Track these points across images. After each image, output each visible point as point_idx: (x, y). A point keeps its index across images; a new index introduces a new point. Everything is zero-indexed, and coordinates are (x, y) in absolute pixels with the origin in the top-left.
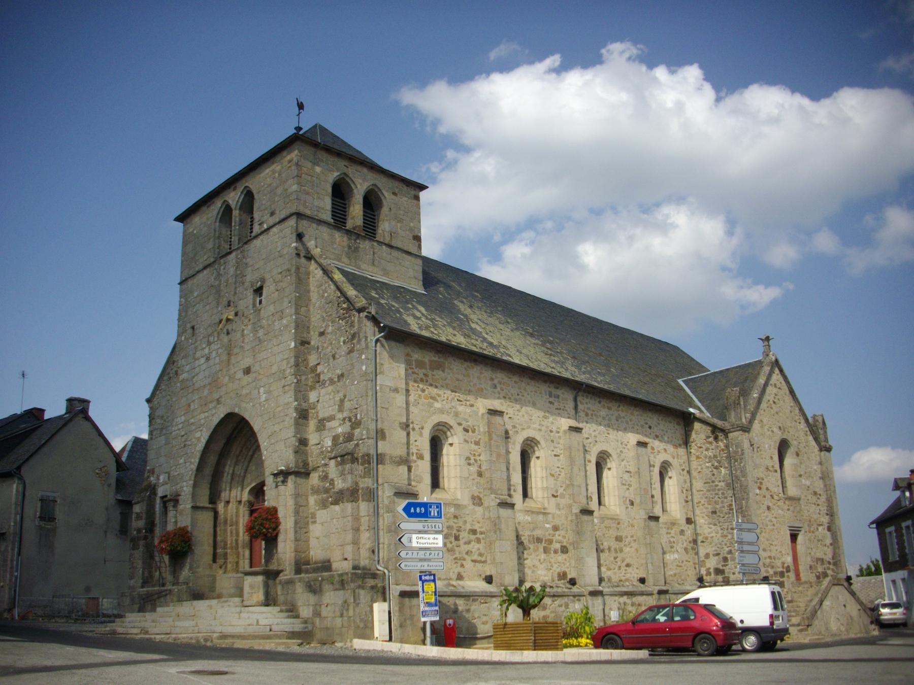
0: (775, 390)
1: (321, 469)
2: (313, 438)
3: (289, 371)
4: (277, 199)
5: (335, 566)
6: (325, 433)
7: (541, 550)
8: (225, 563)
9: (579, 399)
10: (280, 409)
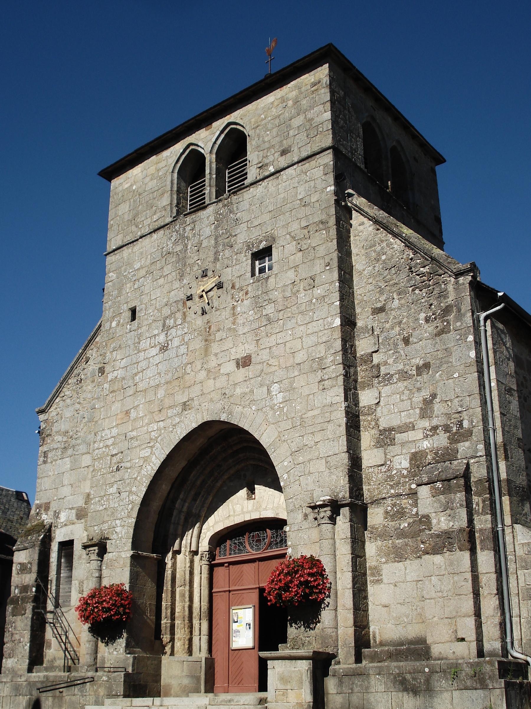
1: (389, 501)
4: (291, 133)
5: (436, 650)
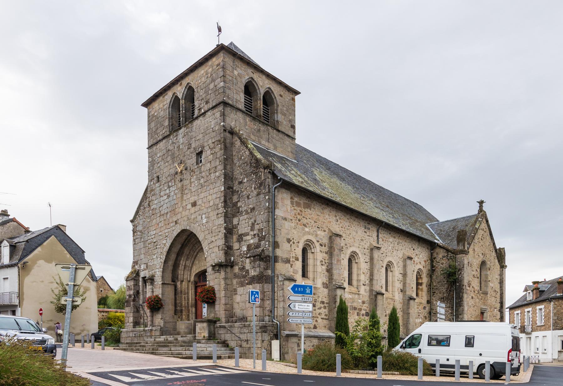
0: (483, 232)
2: (236, 246)
3: (220, 204)
4: (210, 92)
6: (243, 243)
7: (356, 314)
8: (182, 315)
9: (380, 231)
10: (216, 227)
